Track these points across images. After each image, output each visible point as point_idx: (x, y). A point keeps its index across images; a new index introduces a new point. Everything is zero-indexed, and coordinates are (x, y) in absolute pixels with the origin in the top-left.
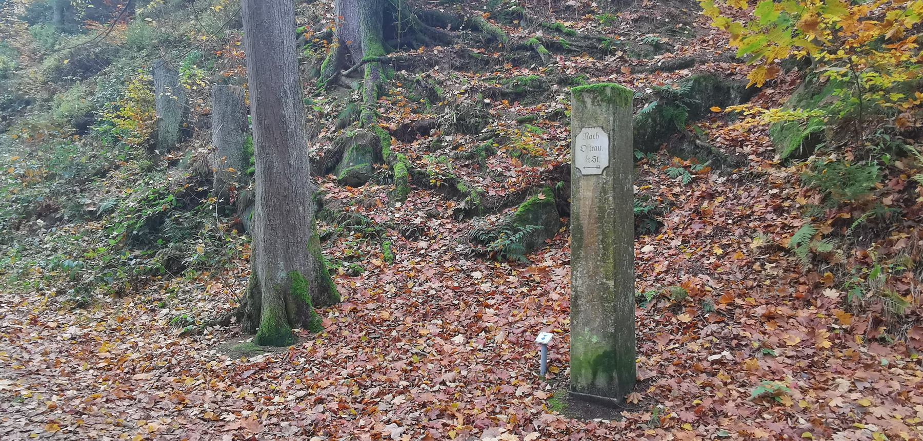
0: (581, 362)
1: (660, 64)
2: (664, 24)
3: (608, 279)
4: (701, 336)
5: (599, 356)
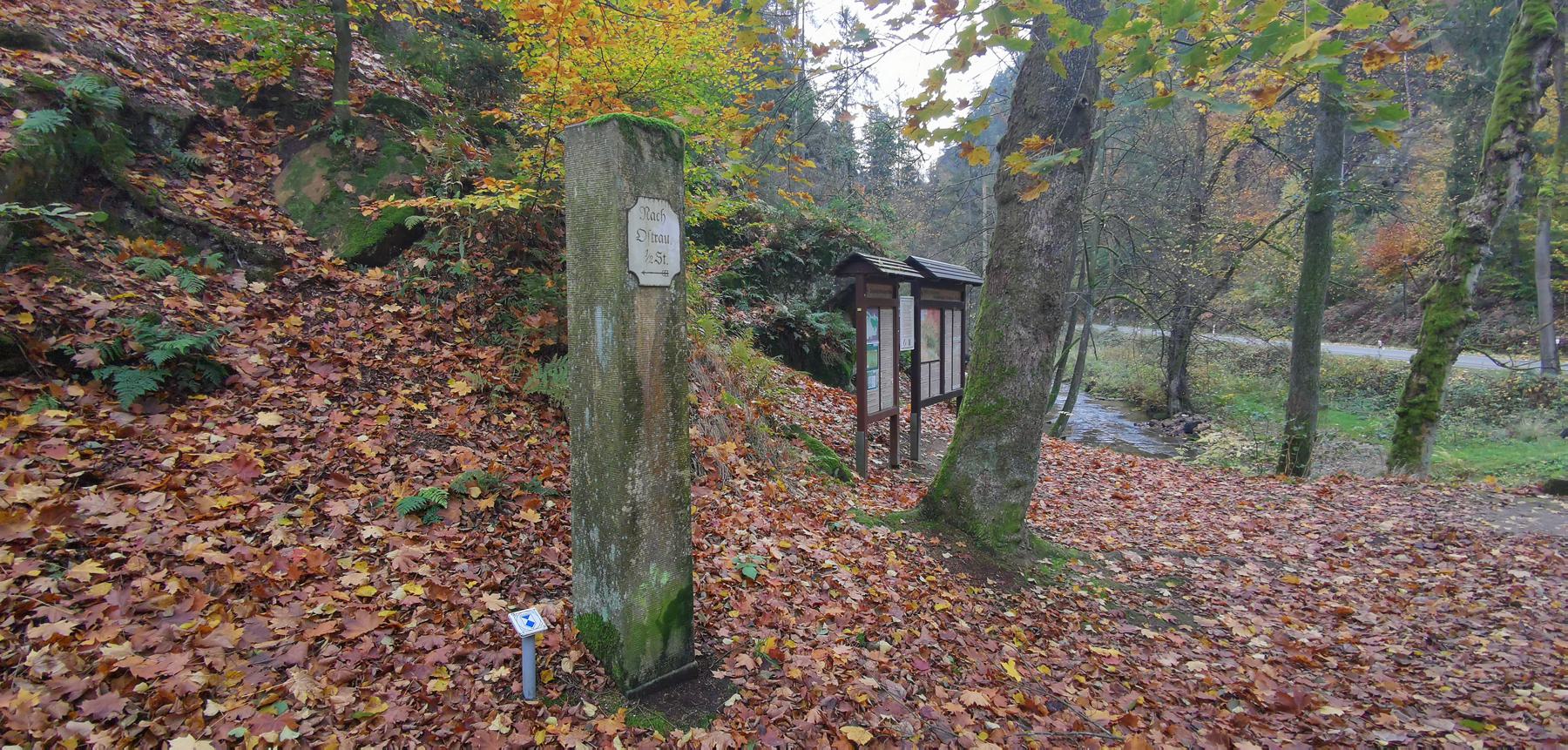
0: (644, 628)
3: (681, 468)
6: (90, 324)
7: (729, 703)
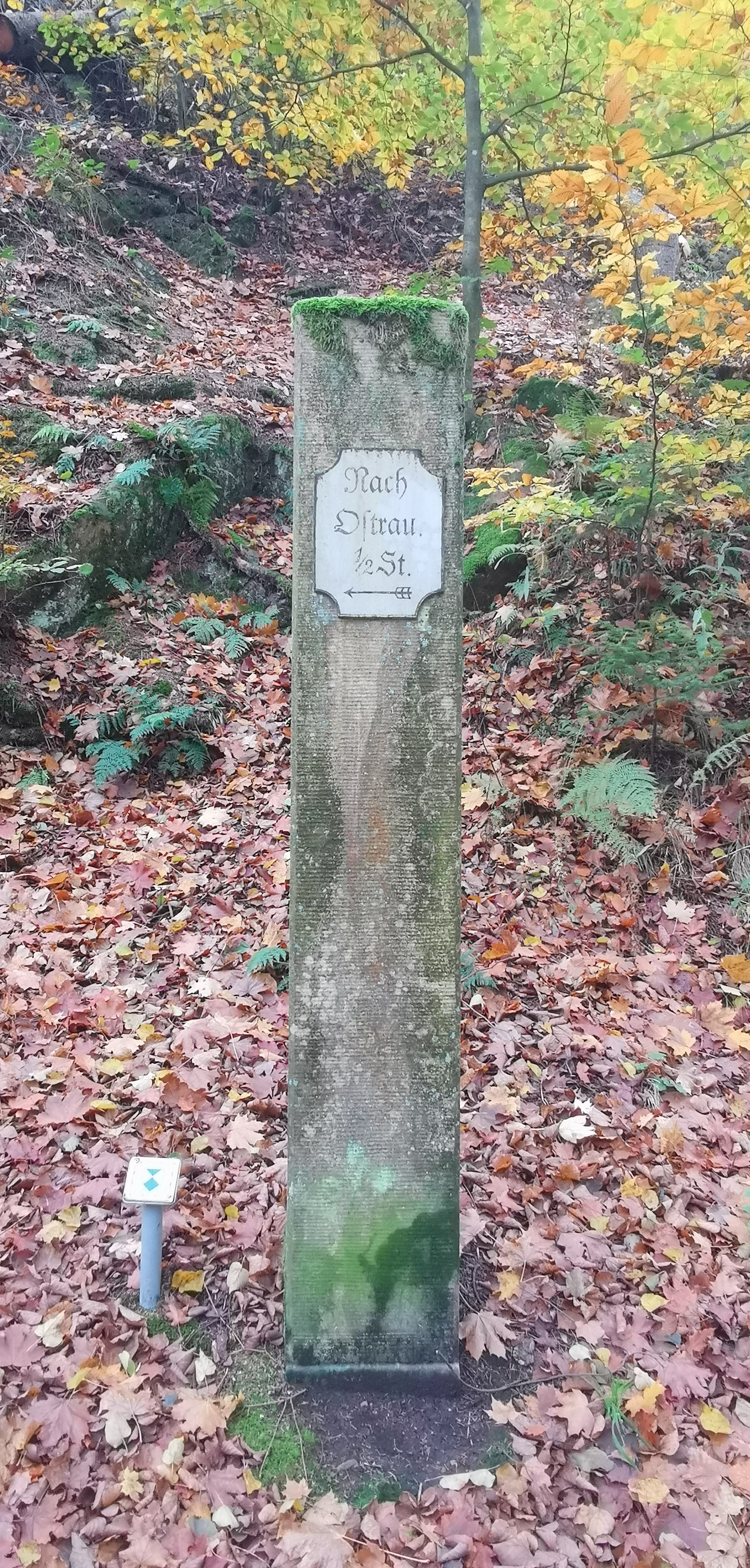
0: (330, 1262)
1: (118, 382)
2: (103, 300)
3: (433, 974)
4: (499, 1062)
5: (398, 1236)
6: (108, 691)
7: (452, 1482)
